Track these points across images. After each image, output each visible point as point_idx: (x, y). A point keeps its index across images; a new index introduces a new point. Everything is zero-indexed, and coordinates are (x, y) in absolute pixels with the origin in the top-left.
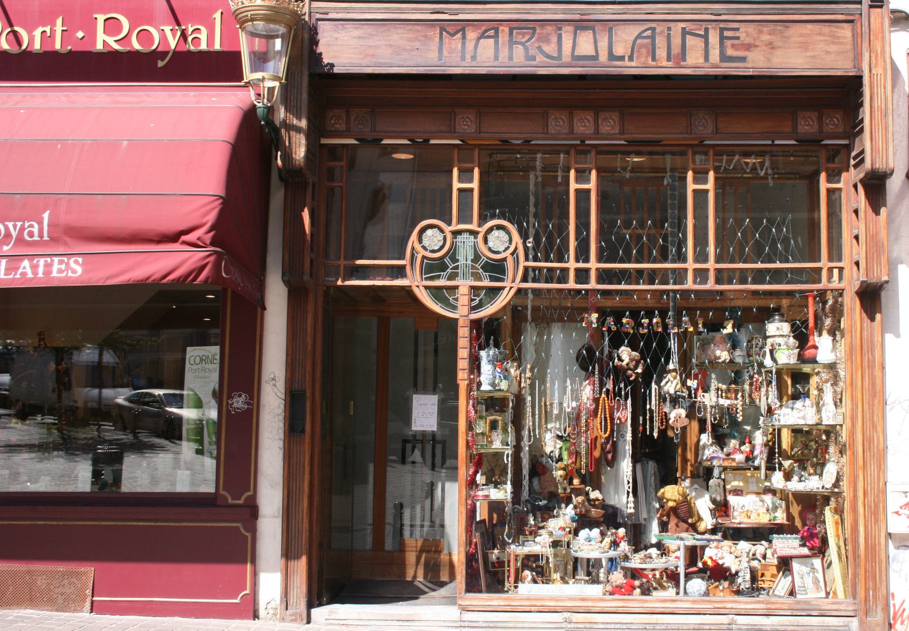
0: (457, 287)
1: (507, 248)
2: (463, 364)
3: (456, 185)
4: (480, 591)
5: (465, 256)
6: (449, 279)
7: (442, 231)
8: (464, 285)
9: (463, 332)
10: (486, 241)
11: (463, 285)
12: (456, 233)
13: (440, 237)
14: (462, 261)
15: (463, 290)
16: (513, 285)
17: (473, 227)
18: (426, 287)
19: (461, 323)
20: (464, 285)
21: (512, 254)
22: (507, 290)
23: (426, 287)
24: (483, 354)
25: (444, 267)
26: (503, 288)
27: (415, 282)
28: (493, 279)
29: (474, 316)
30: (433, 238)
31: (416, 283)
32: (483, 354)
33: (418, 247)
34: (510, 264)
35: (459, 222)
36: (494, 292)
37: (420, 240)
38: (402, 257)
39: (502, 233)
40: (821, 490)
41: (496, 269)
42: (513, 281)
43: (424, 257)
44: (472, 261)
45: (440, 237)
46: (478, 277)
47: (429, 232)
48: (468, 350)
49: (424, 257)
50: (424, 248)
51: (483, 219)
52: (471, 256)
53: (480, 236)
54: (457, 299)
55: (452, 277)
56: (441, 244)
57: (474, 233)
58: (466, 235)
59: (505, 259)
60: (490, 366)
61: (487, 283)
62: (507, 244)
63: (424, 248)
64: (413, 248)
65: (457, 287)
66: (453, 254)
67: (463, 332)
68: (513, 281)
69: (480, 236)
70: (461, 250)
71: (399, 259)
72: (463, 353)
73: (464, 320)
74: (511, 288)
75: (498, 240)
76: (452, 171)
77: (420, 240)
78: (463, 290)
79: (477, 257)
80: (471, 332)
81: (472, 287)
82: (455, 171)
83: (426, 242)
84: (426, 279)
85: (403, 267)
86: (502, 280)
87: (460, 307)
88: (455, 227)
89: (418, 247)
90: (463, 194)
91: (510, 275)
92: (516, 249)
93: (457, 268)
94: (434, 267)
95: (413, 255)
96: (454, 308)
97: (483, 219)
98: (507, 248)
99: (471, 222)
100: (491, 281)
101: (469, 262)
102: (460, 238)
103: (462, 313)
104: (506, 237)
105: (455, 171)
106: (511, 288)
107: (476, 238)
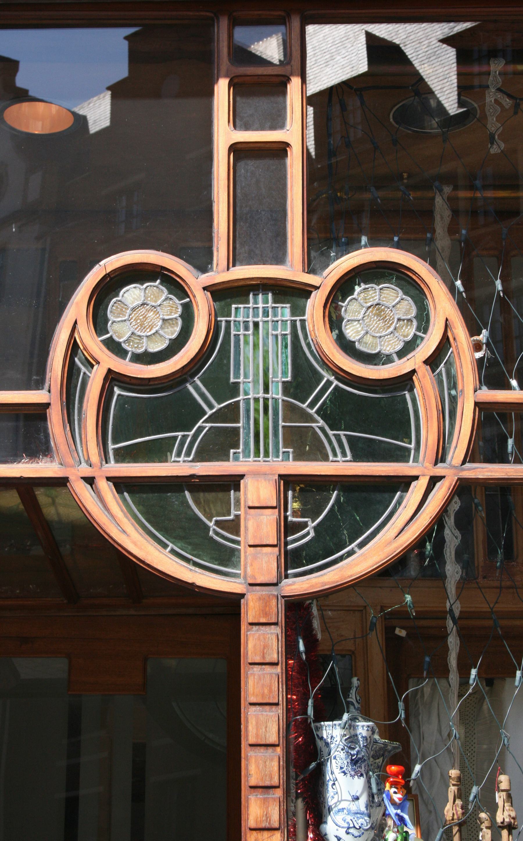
0: (234, 482)
1: (409, 347)
2: (262, 766)
3: (225, 135)
4: (508, 462)
5: (260, 370)
6: (203, 455)
7: (175, 286)
8: (259, 477)
9: (261, 643)
10: (335, 322)
11: (257, 474)
12: (225, 294)
13: (173, 308)
14: (250, 390)
15: (259, 489)
16: (440, 470)
17: (291, 269)
18: (121, 484)
19: (251, 610)
20: (259, 477)
21: (432, 362)
22: (417, 489)
23: (121, 484)
24: (333, 732)
25: (186, 414)
26: (404, 483)
27: (86, 473)
28: (362, 451)
29: (298, 585)
30: (143, 316)
31: (85, 470)
32: (333, 732)
33: (91, 341)
34: (425, 396)
35: (234, 260)
36: (369, 499)
37: (99, 322)
38: (36, 379)
39: (390, 295)
40: (259, 479)
41: (376, 412)
42: (440, 457)
43: (113, 378)
44: (287, 388)
45: (173, 308)
46: (304, 444)
47: (132, 294)
48: (280, 711)
49: (113, 378)
50: (114, 347)
51: (323, 240)
52: (281, 373)
53: (315, 305)
54: (234, 527)
55: (221, 444)
56: (173, 332)
57: (292, 293)
58: (262, 301)
59: (406, 380)
60: (358, 784)
61: (340, 465)
62: (411, 331)
63: (114, 347)
64: (73, 347)
65: (234, 482)
66: (215, 362)
67: (261, 643)
68: (440, 457)
69: (315, 305)
70: (247, 352)
71: (27, 387)
72: (262, 724)
73: (265, 601)
74: (434, 480)
75: (377, 320)
76: (210, 94)
77: (99, 322)
78: (259, 489)
79: (303, 378)
80: (290, 648)
81: (288, 481)
82: (222, 89)
83: (120, 329)
84: (122, 456)
85: (38, 414)
86: (401, 455)
87: (246, 554)
88: (221, 273)
89: (91, 341)
90: (249, 165)
91: (429, 435)
92: (445, 343)
93: (231, 413)
94: (148, 411)
95: (71, 372)
96: (224, 557)
97: (323, 240)
98: (409, 347)
99: (279, 257)
100: (357, 457)
101: (277, 393)
102: (240, 313)
103: (254, 573)
104: (408, 307)
105: (222, 89)
106: (434, 480)
107: (298, 310)
